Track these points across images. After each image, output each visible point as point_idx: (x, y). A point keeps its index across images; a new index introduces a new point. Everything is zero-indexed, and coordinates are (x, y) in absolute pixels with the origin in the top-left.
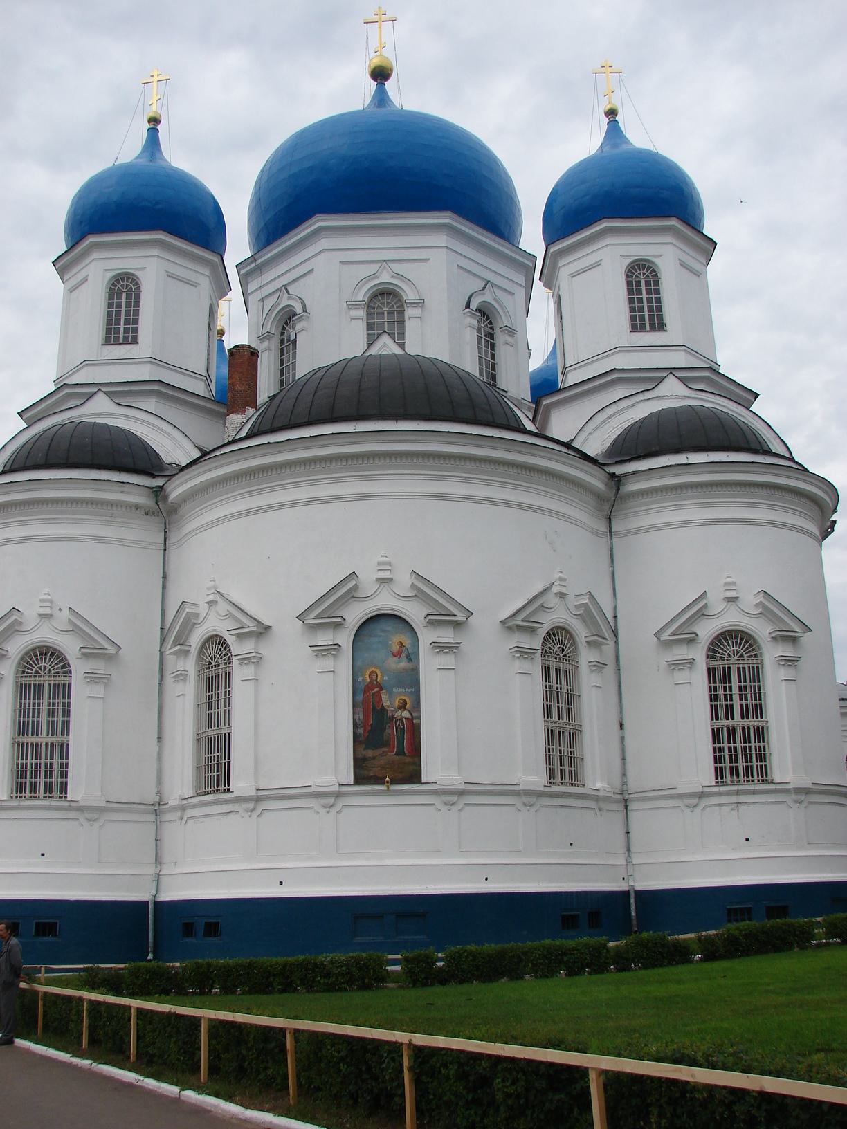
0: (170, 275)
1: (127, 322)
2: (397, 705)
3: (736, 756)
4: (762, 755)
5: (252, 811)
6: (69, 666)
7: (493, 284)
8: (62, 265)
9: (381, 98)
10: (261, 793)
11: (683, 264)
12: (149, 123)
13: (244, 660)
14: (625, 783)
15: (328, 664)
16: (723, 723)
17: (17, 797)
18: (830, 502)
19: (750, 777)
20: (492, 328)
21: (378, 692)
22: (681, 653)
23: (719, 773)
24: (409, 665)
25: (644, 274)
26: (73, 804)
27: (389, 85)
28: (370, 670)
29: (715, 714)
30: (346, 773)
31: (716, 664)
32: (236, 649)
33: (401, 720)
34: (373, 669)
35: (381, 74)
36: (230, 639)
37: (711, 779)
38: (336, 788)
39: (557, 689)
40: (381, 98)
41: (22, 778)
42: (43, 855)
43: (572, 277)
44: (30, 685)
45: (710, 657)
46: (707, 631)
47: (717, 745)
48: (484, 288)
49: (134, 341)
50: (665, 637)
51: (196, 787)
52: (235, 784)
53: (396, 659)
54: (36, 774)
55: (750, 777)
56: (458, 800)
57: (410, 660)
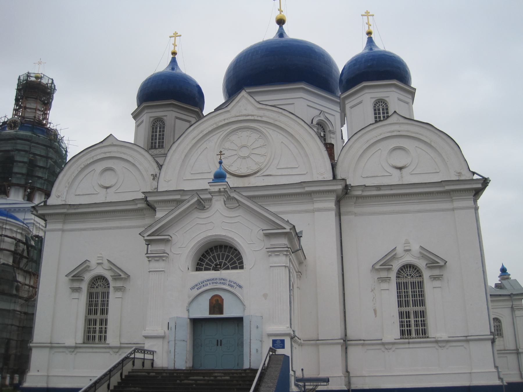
0: (308, 106)
1: (159, 139)
5: (117, 352)
6: (396, 276)
7: (324, 112)
8: (136, 115)
9: (281, 34)
10: (77, 345)
11: (399, 100)
12: (172, 55)
13: (117, 289)
14: (346, 335)
16: (103, 317)
19: (93, 341)
22: (384, 274)
27: (284, 26)
35: (281, 22)
36: (110, 279)
37: (398, 335)
40: (281, 34)
42: (38, 371)
43: (351, 108)
44: (401, 283)
45: (398, 277)
46: (396, 265)
47: (100, 326)
48: (320, 114)
49: (162, 147)
50: (378, 267)
55: (93, 341)
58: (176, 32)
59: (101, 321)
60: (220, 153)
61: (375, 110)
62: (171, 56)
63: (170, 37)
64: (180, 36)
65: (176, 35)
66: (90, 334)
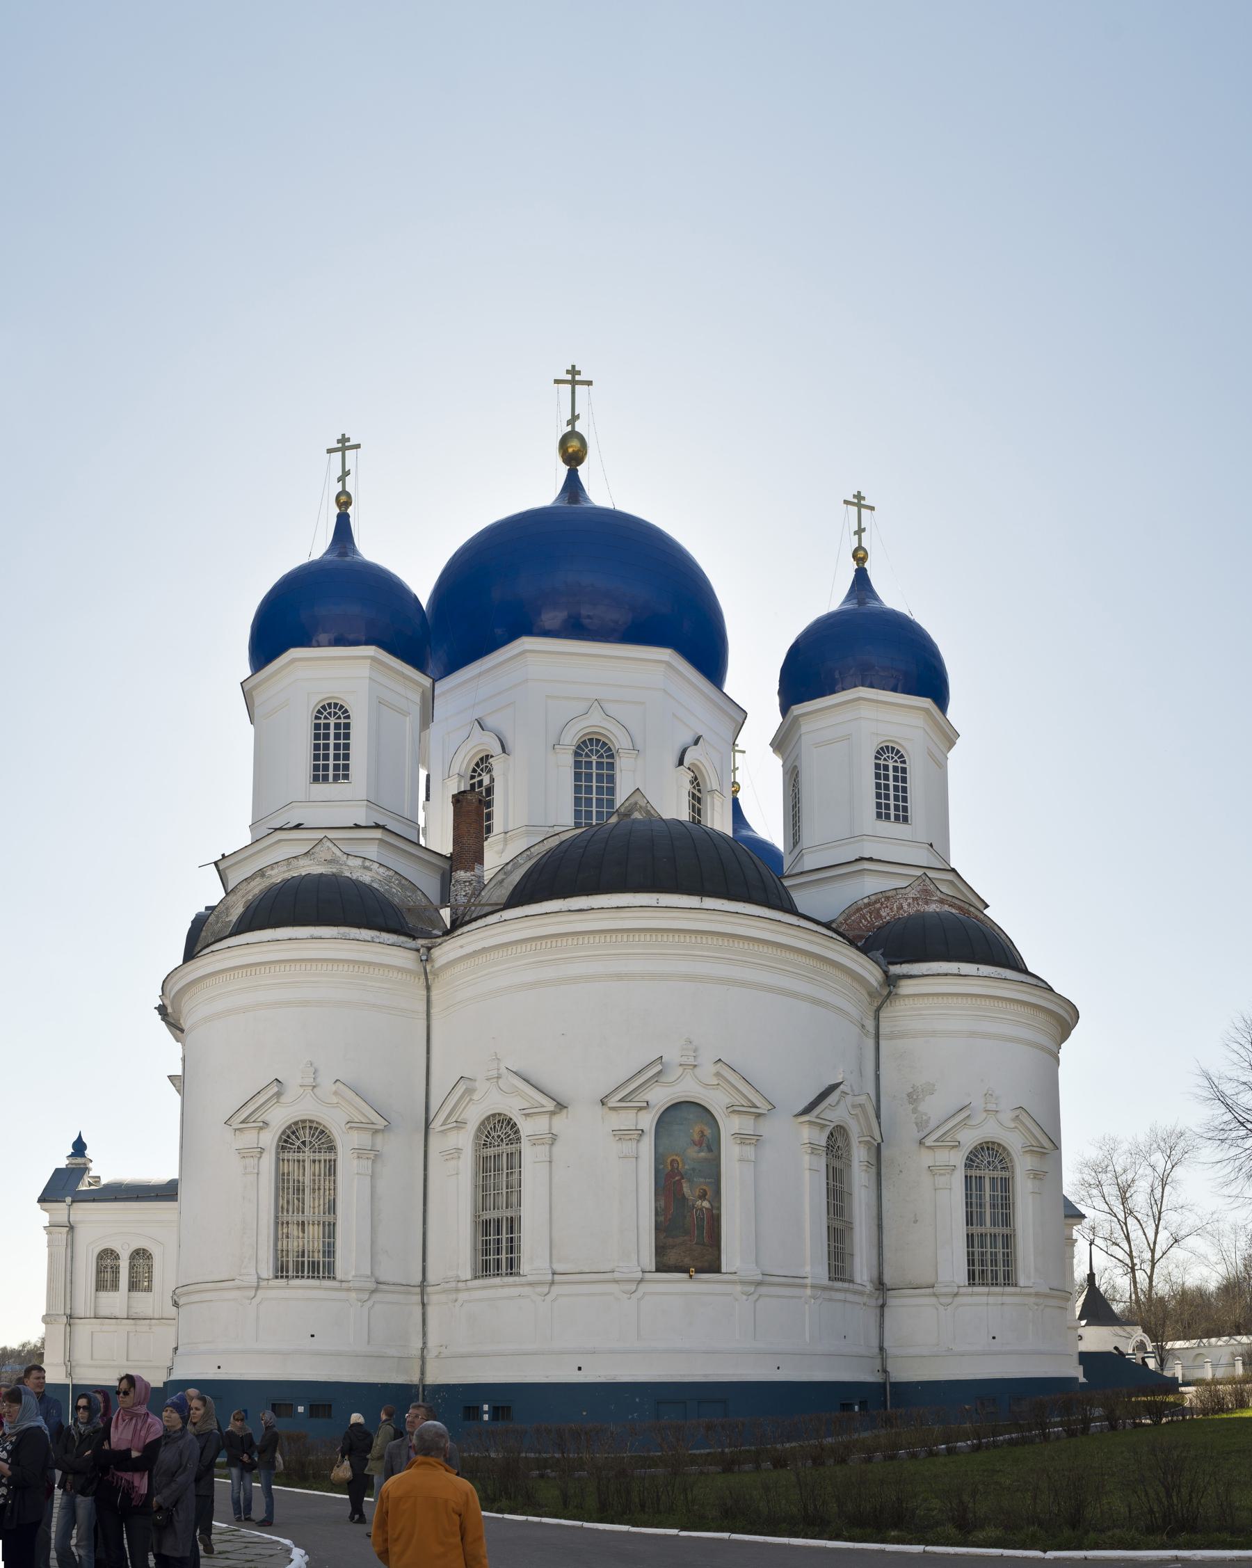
2: (697, 1194)
3: (973, 1260)
4: (1009, 1260)
9: (573, 487)
15: (628, 1147)
17: (483, 1276)
18: (1070, 1021)
20: (699, 791)
21: (679, 1181)
23: (971, 1275)
24: (709, 1155)
25: (893, 758)
26: (344, 1285)
28: (670, 1159)
29: (969, 1221)
30: (649, 1260)
31: (974, 1173)
32: (526, 1127)
33: (701, 1210)
34: (675, 1157)
38: (1048, 1291)
39: (834, 1186)
40: (573, 487)
41: (486, 1256)
51: (475, 1270)
52: (525, 1267)
53: (696, 1148)
54: (994, 1262)
56: (755, 1291)
57: (710, 1150)
58: (343, 435)
59: (974, 1284)
60: (569, 377)
61: (317, 727)
62: (336, 510)
63: (330, 451)
64: (357, 446)
65: (344, 445)
66: (488, 1257)
